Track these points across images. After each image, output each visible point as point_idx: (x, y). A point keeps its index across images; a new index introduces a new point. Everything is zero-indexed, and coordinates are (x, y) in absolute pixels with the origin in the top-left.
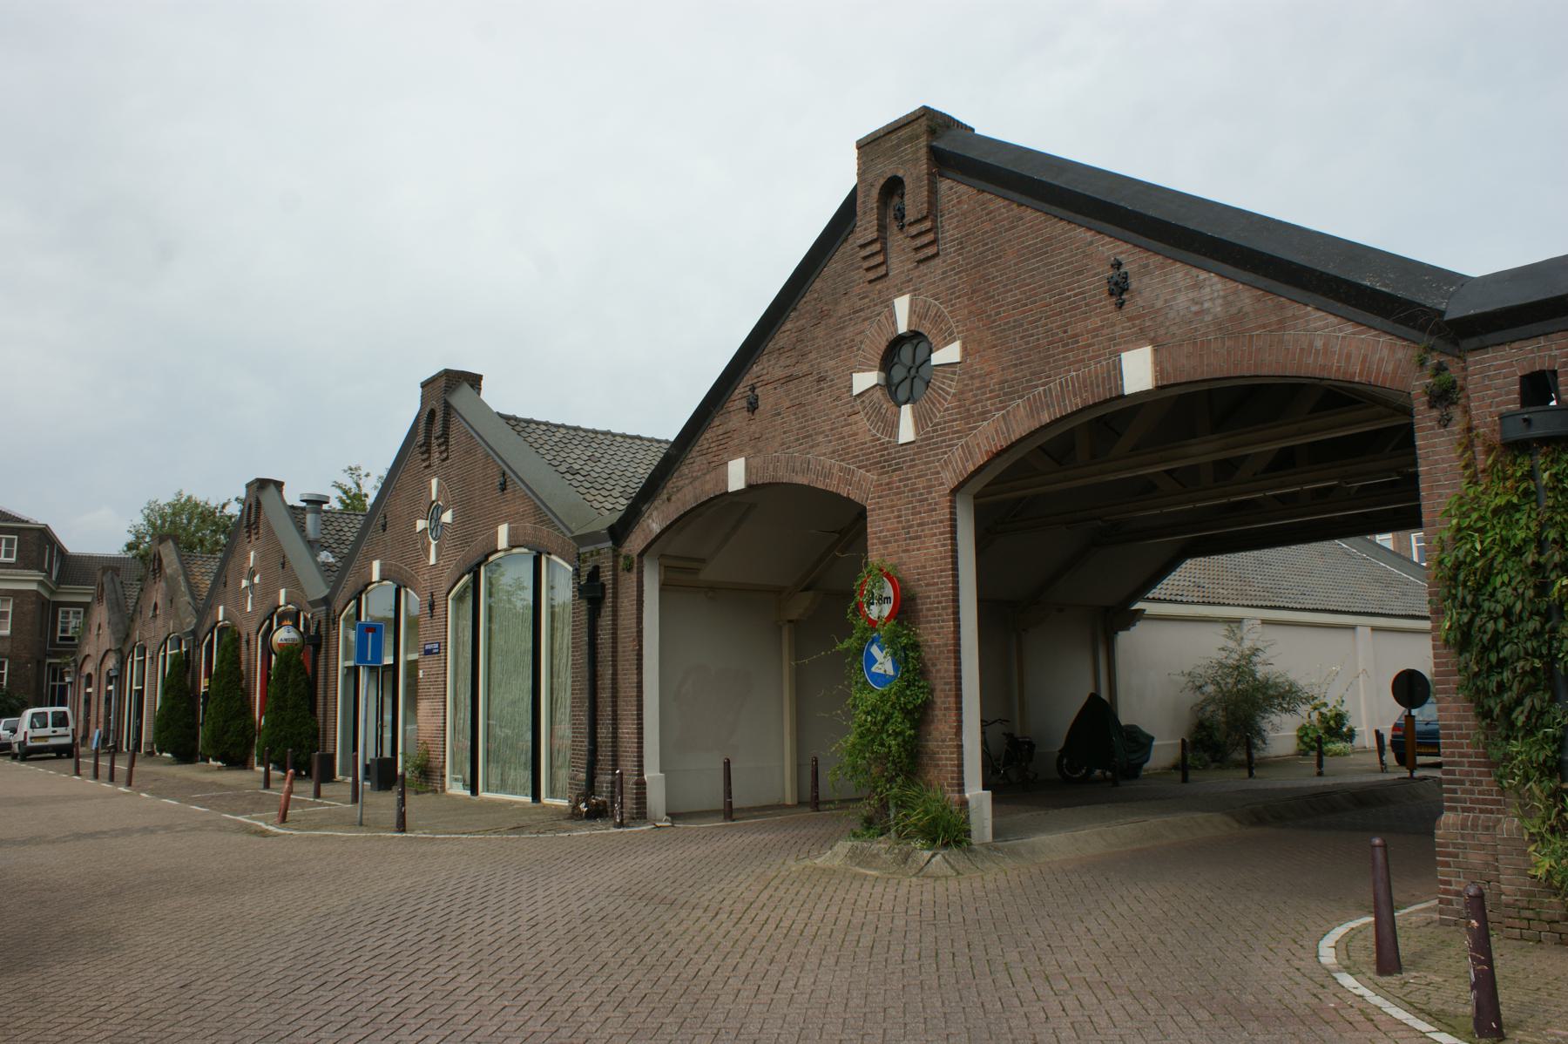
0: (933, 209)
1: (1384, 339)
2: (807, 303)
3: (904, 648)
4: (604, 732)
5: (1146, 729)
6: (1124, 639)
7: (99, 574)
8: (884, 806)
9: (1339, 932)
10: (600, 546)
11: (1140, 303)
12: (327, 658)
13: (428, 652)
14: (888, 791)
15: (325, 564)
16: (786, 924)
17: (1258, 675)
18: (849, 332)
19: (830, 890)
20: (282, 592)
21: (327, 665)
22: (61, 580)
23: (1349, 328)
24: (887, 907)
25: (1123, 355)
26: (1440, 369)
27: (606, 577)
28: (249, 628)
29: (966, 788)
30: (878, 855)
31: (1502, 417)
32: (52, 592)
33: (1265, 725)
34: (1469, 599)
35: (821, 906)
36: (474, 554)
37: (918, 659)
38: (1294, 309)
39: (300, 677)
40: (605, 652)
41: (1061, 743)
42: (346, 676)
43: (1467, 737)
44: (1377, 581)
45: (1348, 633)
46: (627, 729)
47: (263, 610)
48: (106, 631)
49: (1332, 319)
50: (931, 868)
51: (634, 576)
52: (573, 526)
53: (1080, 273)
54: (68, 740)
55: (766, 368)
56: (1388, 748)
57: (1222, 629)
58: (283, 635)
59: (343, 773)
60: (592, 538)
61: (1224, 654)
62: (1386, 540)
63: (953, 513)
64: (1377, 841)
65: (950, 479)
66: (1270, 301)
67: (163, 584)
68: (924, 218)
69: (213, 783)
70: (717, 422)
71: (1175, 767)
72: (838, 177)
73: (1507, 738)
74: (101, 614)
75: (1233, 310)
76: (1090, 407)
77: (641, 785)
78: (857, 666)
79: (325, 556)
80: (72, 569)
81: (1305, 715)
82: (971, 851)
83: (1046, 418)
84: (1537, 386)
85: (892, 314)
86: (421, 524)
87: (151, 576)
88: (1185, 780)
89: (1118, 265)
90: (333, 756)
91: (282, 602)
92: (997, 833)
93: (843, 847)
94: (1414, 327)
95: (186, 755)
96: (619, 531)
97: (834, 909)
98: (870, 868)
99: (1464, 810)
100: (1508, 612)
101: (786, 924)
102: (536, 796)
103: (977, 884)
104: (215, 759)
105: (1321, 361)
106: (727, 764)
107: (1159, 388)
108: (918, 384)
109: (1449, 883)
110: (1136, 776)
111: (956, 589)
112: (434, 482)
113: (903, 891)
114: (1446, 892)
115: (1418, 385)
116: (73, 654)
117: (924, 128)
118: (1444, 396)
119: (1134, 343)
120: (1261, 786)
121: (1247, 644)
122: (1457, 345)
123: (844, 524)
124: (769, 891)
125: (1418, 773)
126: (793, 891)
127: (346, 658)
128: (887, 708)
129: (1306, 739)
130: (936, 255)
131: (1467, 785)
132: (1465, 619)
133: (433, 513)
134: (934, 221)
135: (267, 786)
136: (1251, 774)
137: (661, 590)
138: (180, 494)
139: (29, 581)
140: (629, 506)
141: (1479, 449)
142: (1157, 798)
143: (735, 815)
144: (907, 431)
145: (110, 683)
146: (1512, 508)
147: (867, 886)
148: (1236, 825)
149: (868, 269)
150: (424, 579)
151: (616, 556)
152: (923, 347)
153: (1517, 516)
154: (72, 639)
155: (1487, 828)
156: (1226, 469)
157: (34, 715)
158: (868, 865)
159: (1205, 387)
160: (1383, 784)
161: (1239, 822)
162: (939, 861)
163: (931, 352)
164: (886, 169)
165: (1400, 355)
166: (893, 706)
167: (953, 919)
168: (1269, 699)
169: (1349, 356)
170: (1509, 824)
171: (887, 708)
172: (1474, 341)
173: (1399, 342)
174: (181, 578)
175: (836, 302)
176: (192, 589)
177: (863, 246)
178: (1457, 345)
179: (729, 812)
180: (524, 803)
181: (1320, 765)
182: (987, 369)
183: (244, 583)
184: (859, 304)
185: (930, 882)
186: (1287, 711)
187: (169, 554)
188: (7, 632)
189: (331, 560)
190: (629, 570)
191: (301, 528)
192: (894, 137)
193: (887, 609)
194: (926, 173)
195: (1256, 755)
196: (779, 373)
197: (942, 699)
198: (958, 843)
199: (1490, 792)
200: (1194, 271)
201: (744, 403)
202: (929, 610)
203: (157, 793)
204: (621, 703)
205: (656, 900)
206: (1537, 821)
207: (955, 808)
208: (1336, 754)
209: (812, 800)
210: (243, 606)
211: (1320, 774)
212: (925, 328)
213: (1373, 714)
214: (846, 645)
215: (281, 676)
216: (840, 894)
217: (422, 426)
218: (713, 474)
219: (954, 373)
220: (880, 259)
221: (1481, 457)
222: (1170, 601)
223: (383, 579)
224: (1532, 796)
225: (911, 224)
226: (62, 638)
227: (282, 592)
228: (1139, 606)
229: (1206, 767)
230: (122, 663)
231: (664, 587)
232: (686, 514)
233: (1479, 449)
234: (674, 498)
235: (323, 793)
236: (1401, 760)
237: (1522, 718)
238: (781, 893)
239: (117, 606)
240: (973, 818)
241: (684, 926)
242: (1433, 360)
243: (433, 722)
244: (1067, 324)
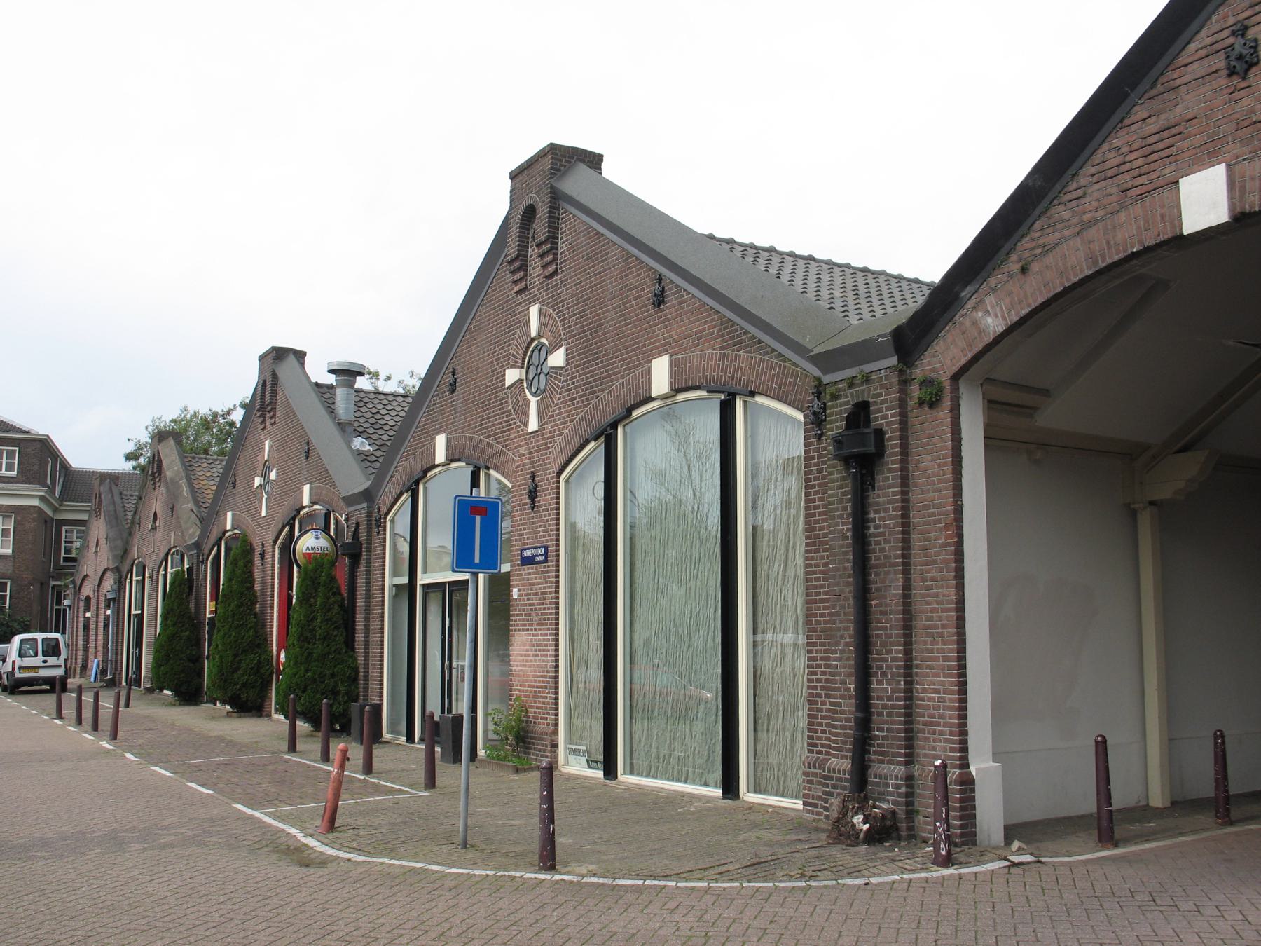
4: (885, 689)
7: (96, 483)
10: (868, 368)
12: (368, 573)
13: (527, 561)
15: (360, 453)
20: (307, 488)
21: (368, 582)
22: (64, 496)
27: (885, 417)
28: (265, 538)
32: (56, 510)
36: (605, 410)
39: (332, 602)
40: (885, 547)
42: (395, 598)
46: (933, 684)
47: (282, 514)
48: (104, 548)
51: (944, 414)
52: (807, 341)
54: (59, 672)
58: (309, 542)
59: (392, 730)
60: (860, 352)
67: (163, 490)
69: (220, 739)
70: (1140, 112)
74: (99, 529)
77: (967, 783)
79: (359, 443)
80: (75, 484)
86: (512, 375)
87: (150, 483)
90: (377, 709)
91: (306, 502)
95: (189, 695)
96: (912, 338)
102: (730, 786)
104: (224, 702)
106: (1101, 746)
112: (534, 311)
116: (72, 574)
127: (395, 573)
133: (532, 355)
135: (292, 748)
137: (986, 446)
138: (186, 409)
139: (30, 497)
145: (108, 607)
150: (519, 456)
151: (904, 382)
154: (74, 560)
157: (22, 642)
174: (183, 482)
176: (195, 494)
180: (709, 799)
183: (258, 481)
187: (170, 454)
188: (9, 551)
189: (368, 448)
190: (933, 403)
191: (330, 408)
203: (149, 756)
204: (919, 638)
210: (255, 513)
215: (305, 597)
217: (514, 231)
223: (450, 460)
226: (66, 559)
227: (307, 488)
230: (120, 583)
231: (993, 441)
232: (1067, 291)
234: (1035, 267)
235: (376, 764)
239: (114, 520)
243: (547, 660)
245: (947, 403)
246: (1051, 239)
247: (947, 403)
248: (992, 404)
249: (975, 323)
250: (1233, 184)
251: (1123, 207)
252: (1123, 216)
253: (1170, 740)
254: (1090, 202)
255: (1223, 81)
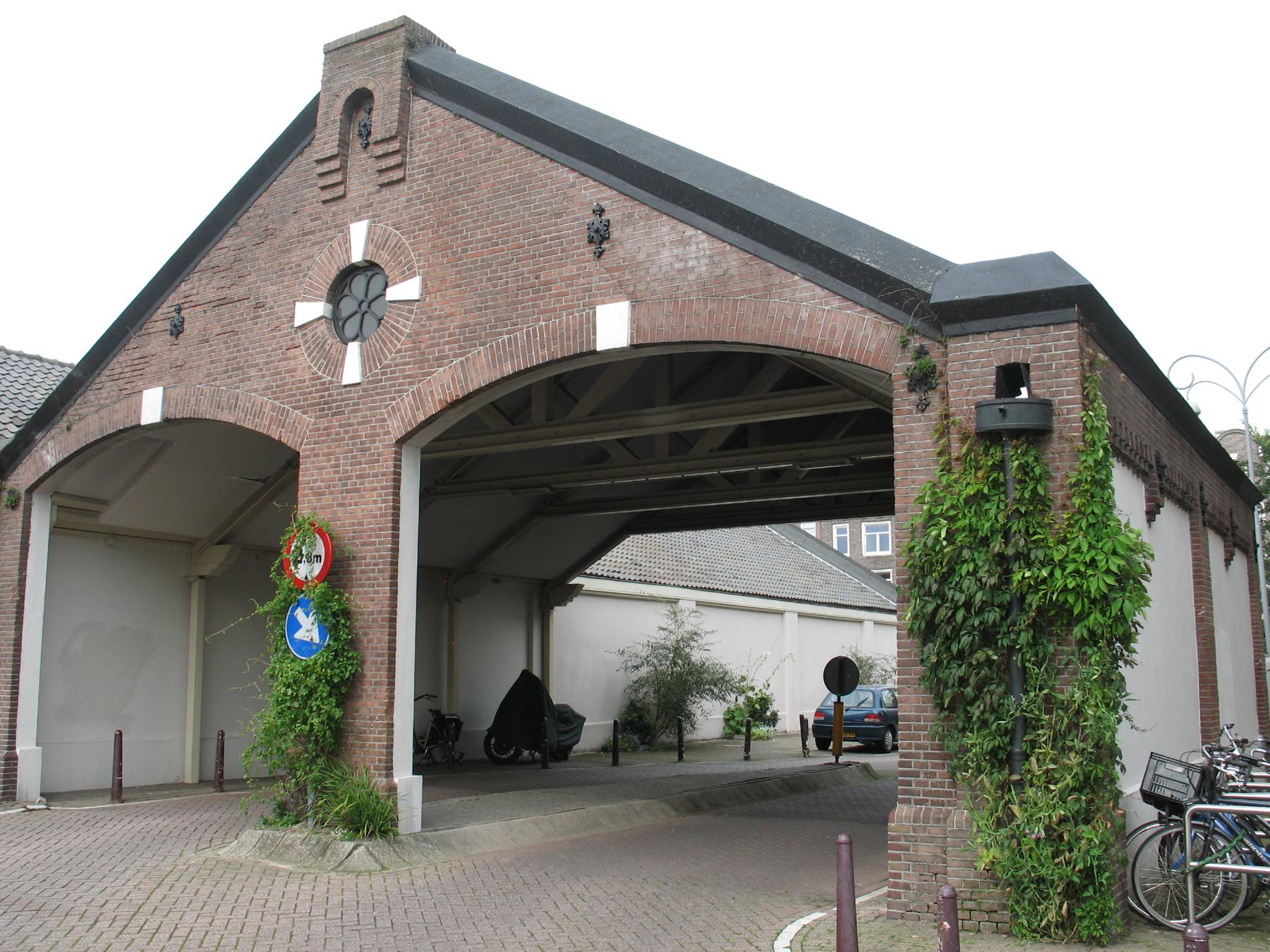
0: (403, 131)
1: (870, 316)
2: (250, 220)
3: (335, 615)
5: (578, 710)
6: (558, 612)
8: (302, 790)
9: (791, 930)
11: (621, 253)
14: (313, 776)
16: (182, 932)
17: (693, 659)
18: (296, 255)
19: (236, 887)
23: (836, 302)
24: (303, 909)
25: (599, 309)
26: (921, 352)
29: (395, 772)
30: (291, 846)
31: (979, 406)
33: (694, 708)
34: (935, 587)
35: (225, 908)
37: (350, 629)
38: (781, 277)
41: (490, 722)
43: (924, 728)
44: (803, 568)
45: (777, 618)
49: (818, 290)
50: (354, 862)
51: (19, 514)
53: (559, 215)
55: (192, 287)
56: (810, 732)
57: (664, 609)
61: (663, 634)
62: (810, 527)
63: (397, 467)
64: (843, 838)
65: (397, 428)
66: (758, 266)
68: (393, 138)
70: (133, 344)
71: (604, 749)
72: (298, 84)
73: (964, 730)
75: (719, 272)
76: (558, 361)
78: (278, 631)
81: (735, 701)
82: (396, 842)
83: (508, 369)
84: (1011, 377)
85: (347, 240)
88: (615, 763)
89: (601, 211)
92: (425, 823)
93: (251, 836)
94: (899, 308)
97: (241, 912)
98: (283, 861)
99: (917, 802)
100: (968, 605)
101: (182, 932)
103: (404, 881)
105: (805, 333)
106: (119, 737)
107: (634, 347)
108: (370, 321)
109: (899, 876)
110: (565, 758)
111: (395, 550)
113: (321, 889)
114: (895, 885)
115: (900, 366)
117: (402, 39)
118: (924, 380)
119: (610, 296)
120: (691, 771)
121: (688, 627)
122: (940, 330)
123: (275, 470)
124: (164, 889)
125: (843, 759)
126: (191, 889)
128: (311, 681)
129: (732, 723)
130: (402, 180)
131: (922, 778)
132: (930, 608)
134: (404, 142)
136: (681, 758)
137: (51, 533)
140: (18, 434)
141: (955, 437)
142: (586, 785)
143: (124, 796)
144: (352, 372)
146: (979, 498)
147: (279, 883)
148: (673, 813)
149: (323, 188)
152: (377, 282)
153: (987, 506)
155: (938, 820)
156: (682, 443)
158: (281, 857)
159: (667, 351)
160: (810, 771)
161: (677, 810)
162: (362, 853)
163: (386, 286)
164: (356, 80)
165: (884, 334)
166: (318, 680)
167: (379, 923)
168: (700, 683)
169: (833, 331)
170: (959, 816)
171: (311, 681)
172: (956, 328)
173: (885, 322)
175: (284, 221)
177: (320, 162)
178: (940, 330)
179: (118, 792)
181: (747, 749)
182: (447, 309)
184: (310, 225)
185: (350, 880)
186: (717, 697)
190: (14, 506)
192: (367, 45)
193: (318, 568)
194: (397, 95)
195: (688, 737)
196: (211, 294)
197: (373, 673)
198: (384, 833)
199: (942, 785)
200: (681, 227)
201: (167, 325)
202: (363, 572)
205: (18, 907)
206: (986, 814)
207: (382, 794)
208: (760, 738)
209: (217, 779)
211: (747, 758)
212: (382, 259)
213: (799, 697)
214: (266, 608)
216: (248, 892)
218: (124, 403)
219: (411, 312)
220: (338, 178)
221: (955, 445)
222: (608, 578)
224: (983, 789)
225: (377, 143)
228: (577, 580)
229: (634, 749)
231: (57, 530)
233: (955, 437)
234: (74, 428)
236: (822, 745)
237: (977, 713)
238: (176, 892)
240: (401, 805)
241: (52, 939)
242: (915, 342)
244: (540, 270)
245: (21, 508)
246: (85, 411)
247: (21, 508)
248: (59, 509)
249: (41, 457)
250: (165, 400)
251: (119, 400)
252: (117, 406)
253: (202, 739)
254: (104, 393)
255: (168, 337)
